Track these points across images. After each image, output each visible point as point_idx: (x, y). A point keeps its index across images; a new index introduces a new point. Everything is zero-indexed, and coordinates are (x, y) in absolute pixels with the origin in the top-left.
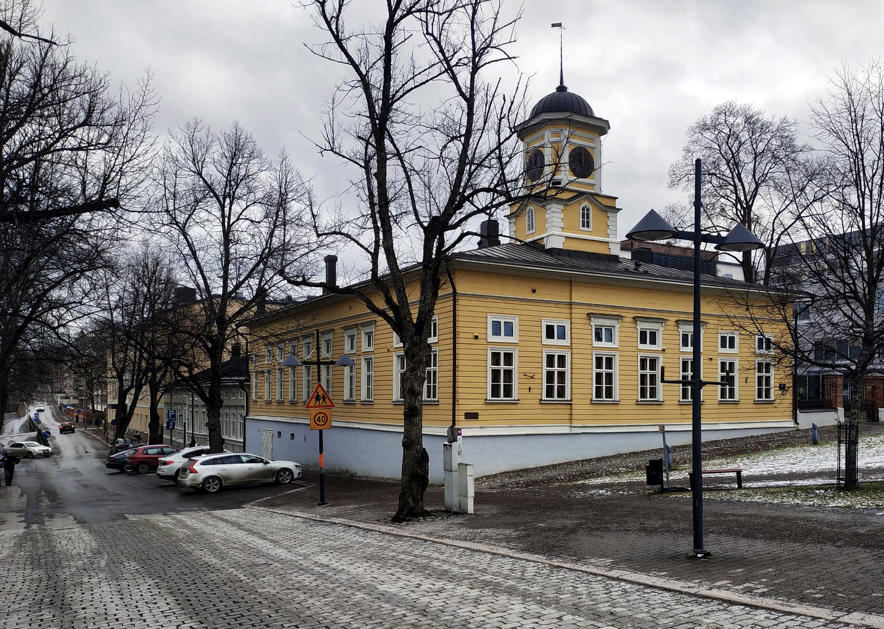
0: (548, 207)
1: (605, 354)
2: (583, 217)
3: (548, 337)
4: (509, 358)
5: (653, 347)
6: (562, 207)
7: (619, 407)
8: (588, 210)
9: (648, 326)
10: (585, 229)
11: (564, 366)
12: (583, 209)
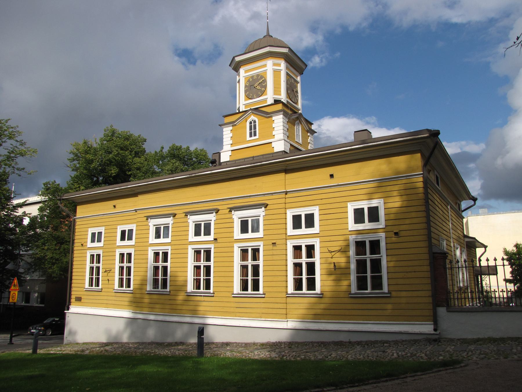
2: (251, 129)
4: (310, 249)
5: (310, 231)
6: (231, 128)
8: (255, 122)
10: (253, 138)
12: (251, 123)
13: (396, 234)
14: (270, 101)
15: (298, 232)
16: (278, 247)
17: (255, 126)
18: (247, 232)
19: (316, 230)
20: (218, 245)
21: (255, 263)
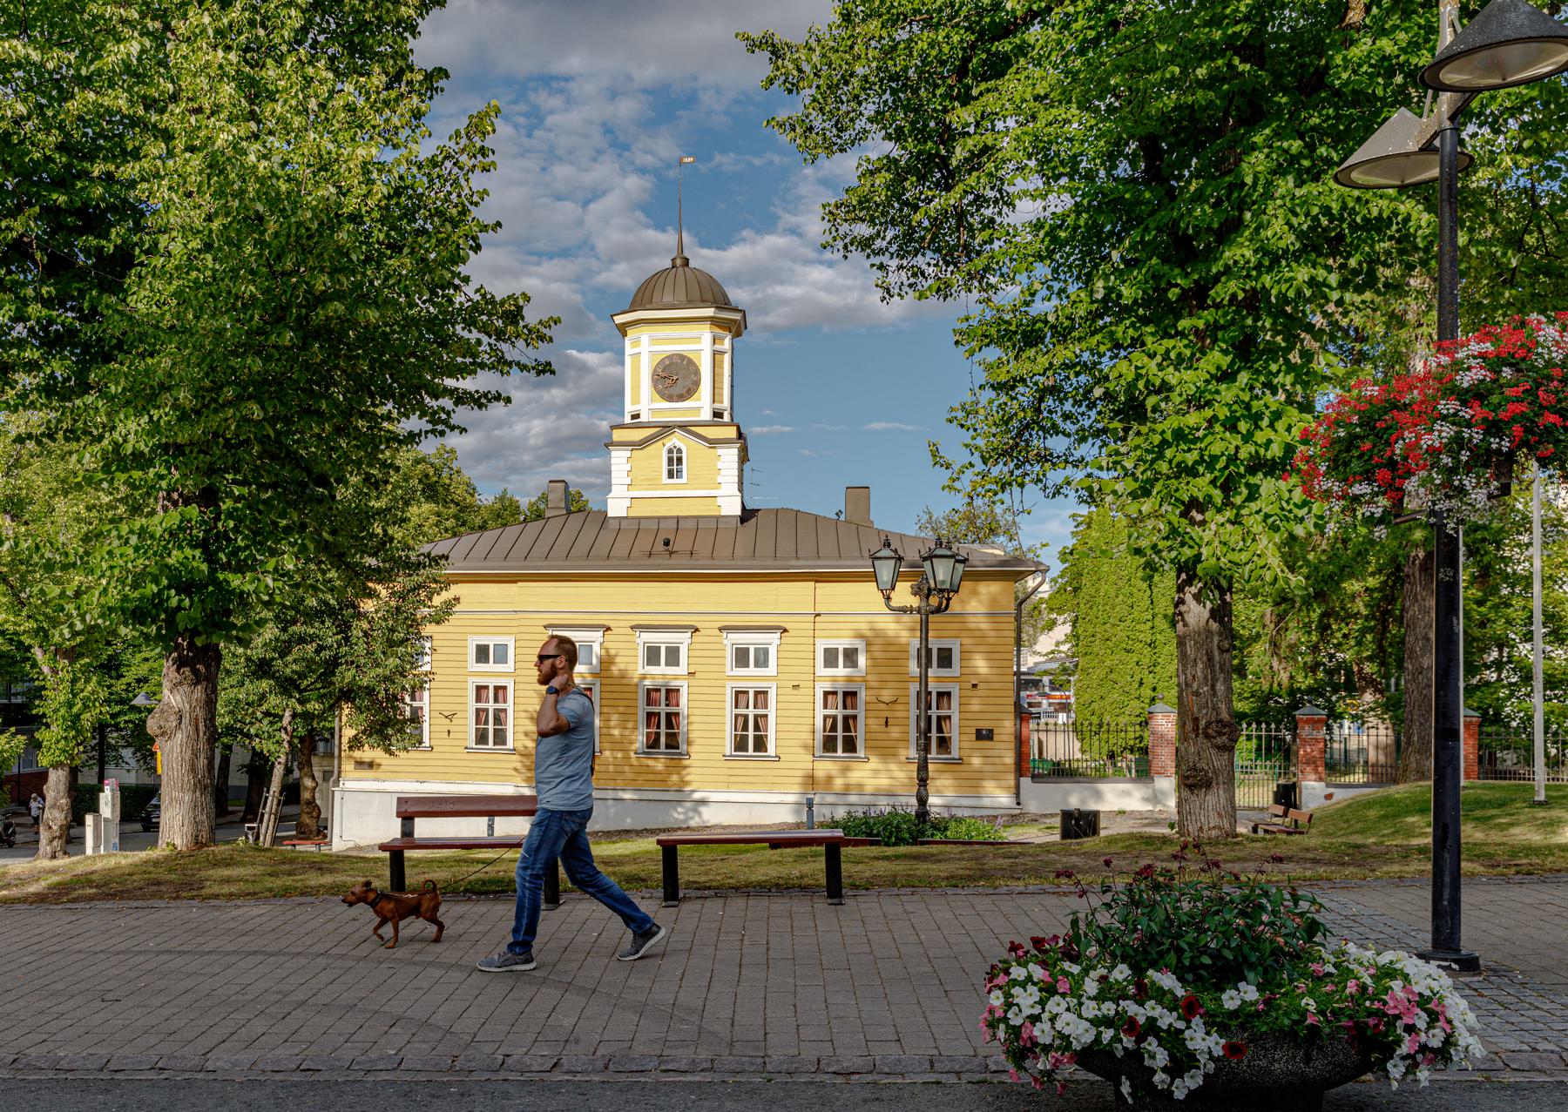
0: (719, 451)
1: (751, 686)
3: (479, 660)
5: (500, 667)
6: (628, 454)
7: (961, 768)
8: (679, 451)
9: (662, 639)
10: (675, 480)
11: (854, 707)
12: (670, 451)
13: (974, 686)
14: (706, 415)
15: (482, 667)
16: (801, 691)
17: (680, 460)
18: (487, 661)
19: (509, 667)
20: (693, 682)
21: (760, 711)
